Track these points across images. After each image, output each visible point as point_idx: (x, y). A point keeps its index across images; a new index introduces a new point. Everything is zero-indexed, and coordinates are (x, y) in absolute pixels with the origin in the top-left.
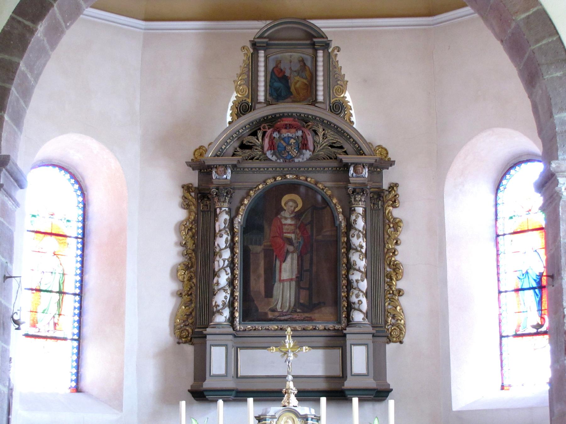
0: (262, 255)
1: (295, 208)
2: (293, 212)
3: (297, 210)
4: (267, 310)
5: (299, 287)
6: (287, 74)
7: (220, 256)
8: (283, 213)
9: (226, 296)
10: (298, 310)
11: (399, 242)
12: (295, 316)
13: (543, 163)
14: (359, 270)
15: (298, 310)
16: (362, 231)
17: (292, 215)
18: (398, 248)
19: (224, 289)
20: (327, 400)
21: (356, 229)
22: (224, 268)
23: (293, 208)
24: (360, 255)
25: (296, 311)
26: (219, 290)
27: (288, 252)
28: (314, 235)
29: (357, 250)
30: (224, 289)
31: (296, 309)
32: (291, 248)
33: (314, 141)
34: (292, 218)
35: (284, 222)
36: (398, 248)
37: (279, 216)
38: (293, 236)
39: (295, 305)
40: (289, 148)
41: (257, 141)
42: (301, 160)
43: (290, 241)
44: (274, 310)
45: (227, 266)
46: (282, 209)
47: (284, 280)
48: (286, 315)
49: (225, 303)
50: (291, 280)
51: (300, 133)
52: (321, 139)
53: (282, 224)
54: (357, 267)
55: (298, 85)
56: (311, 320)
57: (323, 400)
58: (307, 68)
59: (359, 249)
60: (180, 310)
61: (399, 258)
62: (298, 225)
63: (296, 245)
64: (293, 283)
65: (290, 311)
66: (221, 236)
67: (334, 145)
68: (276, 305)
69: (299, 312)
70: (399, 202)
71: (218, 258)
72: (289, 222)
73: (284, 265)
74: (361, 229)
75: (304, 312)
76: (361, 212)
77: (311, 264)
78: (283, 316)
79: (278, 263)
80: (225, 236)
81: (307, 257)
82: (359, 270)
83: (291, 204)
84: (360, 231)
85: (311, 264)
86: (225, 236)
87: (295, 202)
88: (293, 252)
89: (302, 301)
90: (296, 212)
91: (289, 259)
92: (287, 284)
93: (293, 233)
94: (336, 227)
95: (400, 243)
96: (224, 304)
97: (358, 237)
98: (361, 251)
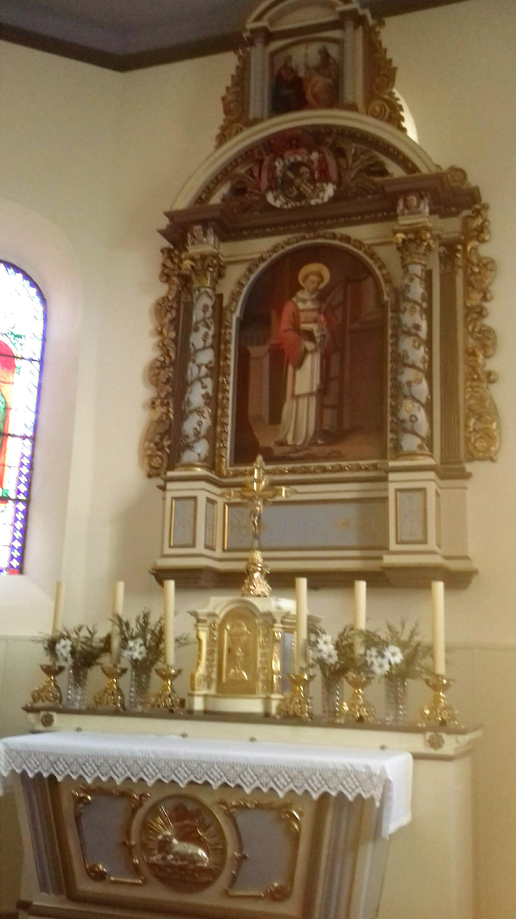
0: (266, 361)
1: (318, 284)
2: (316, 290)
3: (322, 286)
4: (272, 444)
5: (321, 407)
6: (302, 74)
7: (194, 361)
8: (300, 294)
9: (201, 422)
10: (320, 442)
11: (488, 296)
12: (315, 450)
13: (467, 471)
14: (413, 366)
15: (320, 442)
16: (420, 301)
17: (314, 296)
18: (486, 305)
19: (199, 411)
20: (368, 586)
21: (409, 300)
22: (199, 379)
23: (315, 285)
24: (414, 341)
25: (316, 444)
26: (191, 412)
27: (306, 352)
28: (348, 321)
29: (409, 334)
30: (199, 411)
31: (317, 440)
32: (309, 346)
33: (339, 167)
34: (313, 300)
35: (301, 306)
36: (486, 305)
37: (294, 299)
38: (314, 327)
39: (315, 434)
40: (298, 181)
41: (252, 179)
42: (319, 201)
43: (310, 335)
44: (282, 443)
45: (206, 376)
46: (300, 288)
47: (298, 397)
48: (300, 451)
49: (199, 433)
50: (310, 394)
51: (315, 156)
52: (350, 161)
53: (297, 309)
54: (409, 362)
55: (316, 89)
56: (340, 456)
57: (362, 586)
58: (332, 61)
59: (413, 331)
60: (497, 445)
61: (489, 322)
62: (323, 310)
63: (318, 341)
64: (313, 401)
65: (307, 443)
66: (197, 330)
67: (372, 169)
68: (286, 435)
69: (321, 445)
70: (489, 232)
71: (191, 364)
72: (310, 305)
73: (299, 373)
74: (419, 299)
75: (329, 443)
76: (419, 273)
77: (342, 370)
78: (297, 451)
79: (290, 369)
80: (203, 330)
81: (335, 359)
82: (413, 366)
83: (313, 278)
84: (416, 302)
85: (342, 370)
86: (203, 330)
87: (320, 275)
88: (312, 352)
89: (326, 427)
90: (320, 290)
91: (308, 360)
92: (303, 403)
93: (315, 321)
94: (381, 305)
95: (492, 298)
96: (197, 434)
97: (413, 311)
98: (417, 335)
